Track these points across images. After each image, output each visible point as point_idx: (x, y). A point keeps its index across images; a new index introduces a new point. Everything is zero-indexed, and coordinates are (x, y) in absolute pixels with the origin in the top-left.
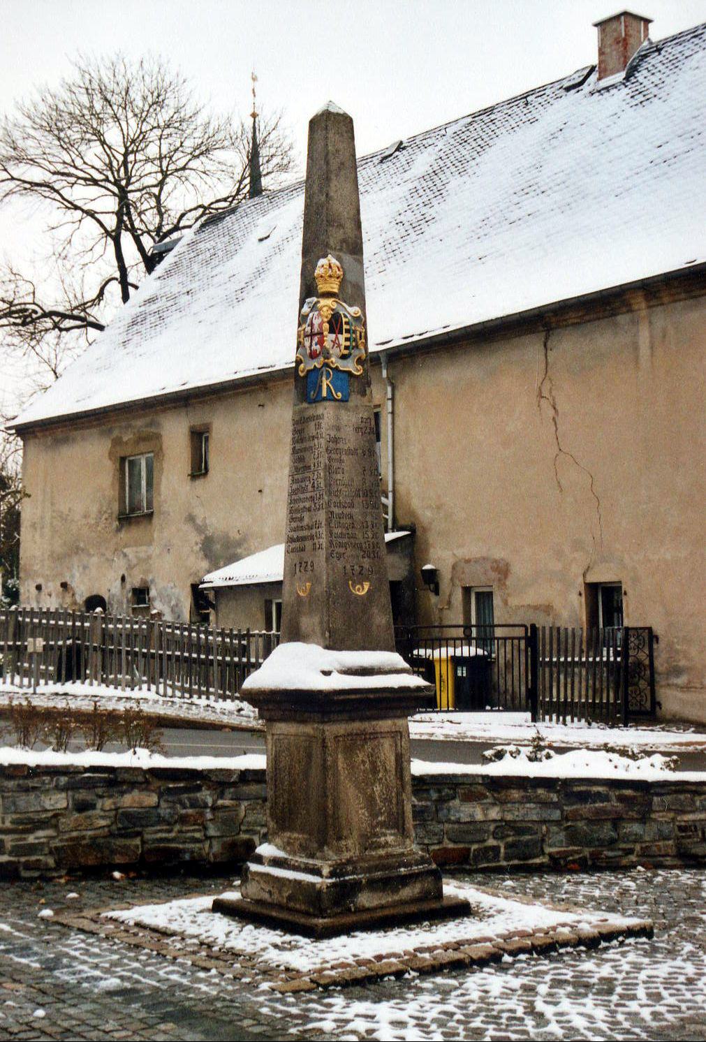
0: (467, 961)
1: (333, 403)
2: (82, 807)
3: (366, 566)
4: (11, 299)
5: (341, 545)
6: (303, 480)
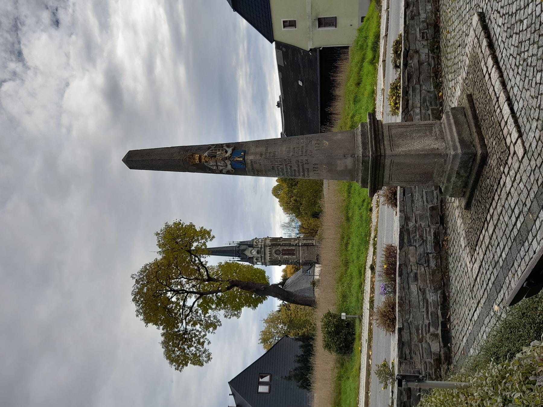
0: (500, 79)
2: (416, 279)
3: (316, 142)
4: (309, 248)
6: (278, 170)
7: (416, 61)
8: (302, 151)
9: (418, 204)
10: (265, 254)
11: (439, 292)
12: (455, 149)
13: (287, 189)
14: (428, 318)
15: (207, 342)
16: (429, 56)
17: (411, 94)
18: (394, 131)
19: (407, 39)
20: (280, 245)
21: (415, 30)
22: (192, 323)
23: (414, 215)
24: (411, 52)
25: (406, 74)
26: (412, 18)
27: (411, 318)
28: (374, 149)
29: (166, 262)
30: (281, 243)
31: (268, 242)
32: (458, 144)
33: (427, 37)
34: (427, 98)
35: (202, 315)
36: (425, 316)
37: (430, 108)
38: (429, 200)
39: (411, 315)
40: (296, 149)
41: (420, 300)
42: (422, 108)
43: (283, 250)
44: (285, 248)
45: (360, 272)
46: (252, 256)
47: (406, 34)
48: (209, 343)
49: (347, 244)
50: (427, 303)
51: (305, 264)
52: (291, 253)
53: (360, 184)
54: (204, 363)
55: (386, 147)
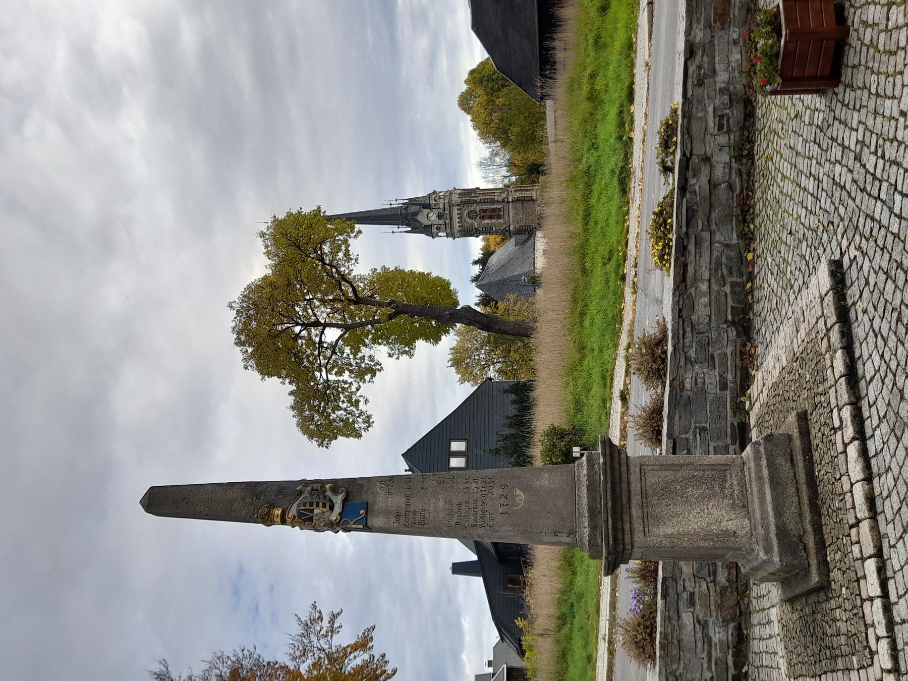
1: (369, 518)
2: (692, 602)
3: (500, 493)
4: (526, 205)
5: (483, 517)
7: (704, 179)
8: (476, 514)
10: (451, 219)
11: (732, 625)
12: (768, 550)
13: (486, 98)
14: (709, 668)
15: (361, 399)
16: (730, 168)
17: (693, 251)
18: (651, 479)
19: (687, 115)
20: (475, 202)
21: (705, 110)
22: (336, 370)
24: (695, 159)
25: (684, 208)
26: (700, 83)
27: (681, 670)
28: (611, 542)
29: (281, 281)
30: (478, 199)
31: (456, 199)
32: (775, 542)
33: (728, 126)
34: (724, 260)
35: (351, 357)
36: (705, 666)
37: (729, 280)
39: (682, 662)
40: (463, 507)
41: (698, 639)
42: (713, 281)
43: (482, 211)
44: (485, 207)
45: (604, 378)
46: (430, 223)
47: (686, 120)
48: (366, 401)
49: (582, 314)
50: (710, 645)
51: (519, 232)
52: (495, 214)
53: (586, 554)
54: (363, 432)
55: (636, 525)
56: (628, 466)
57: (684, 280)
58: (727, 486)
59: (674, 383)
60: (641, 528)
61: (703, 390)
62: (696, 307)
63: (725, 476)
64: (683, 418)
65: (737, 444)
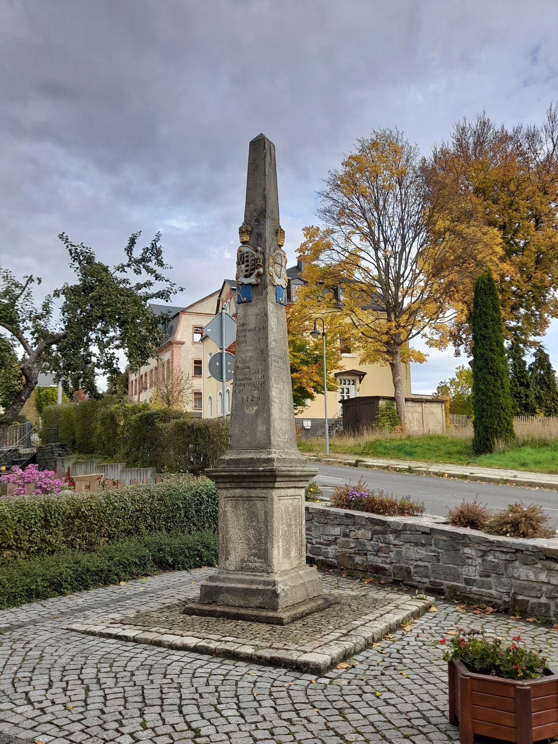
2: (346, 535)
3: (255, 396)
8: (243, 380)
9: (414, 552)
11: (336, 562)
18: (259, 504)
23: (401, 543)
38: (418, 569)
40: (247, 370)
42: (550, 587)
56: (266, 488)
57: (548, 558)
58: (255, 559)
59: (467, 539)
60: (229, 495)
61: (464, 564)
62: (525, 567)
63: (262, 558)
64: (444, 543)
65: (430, 586)
